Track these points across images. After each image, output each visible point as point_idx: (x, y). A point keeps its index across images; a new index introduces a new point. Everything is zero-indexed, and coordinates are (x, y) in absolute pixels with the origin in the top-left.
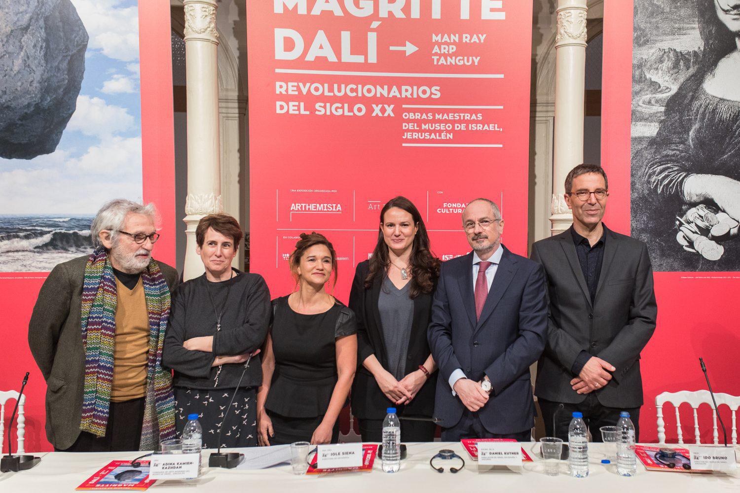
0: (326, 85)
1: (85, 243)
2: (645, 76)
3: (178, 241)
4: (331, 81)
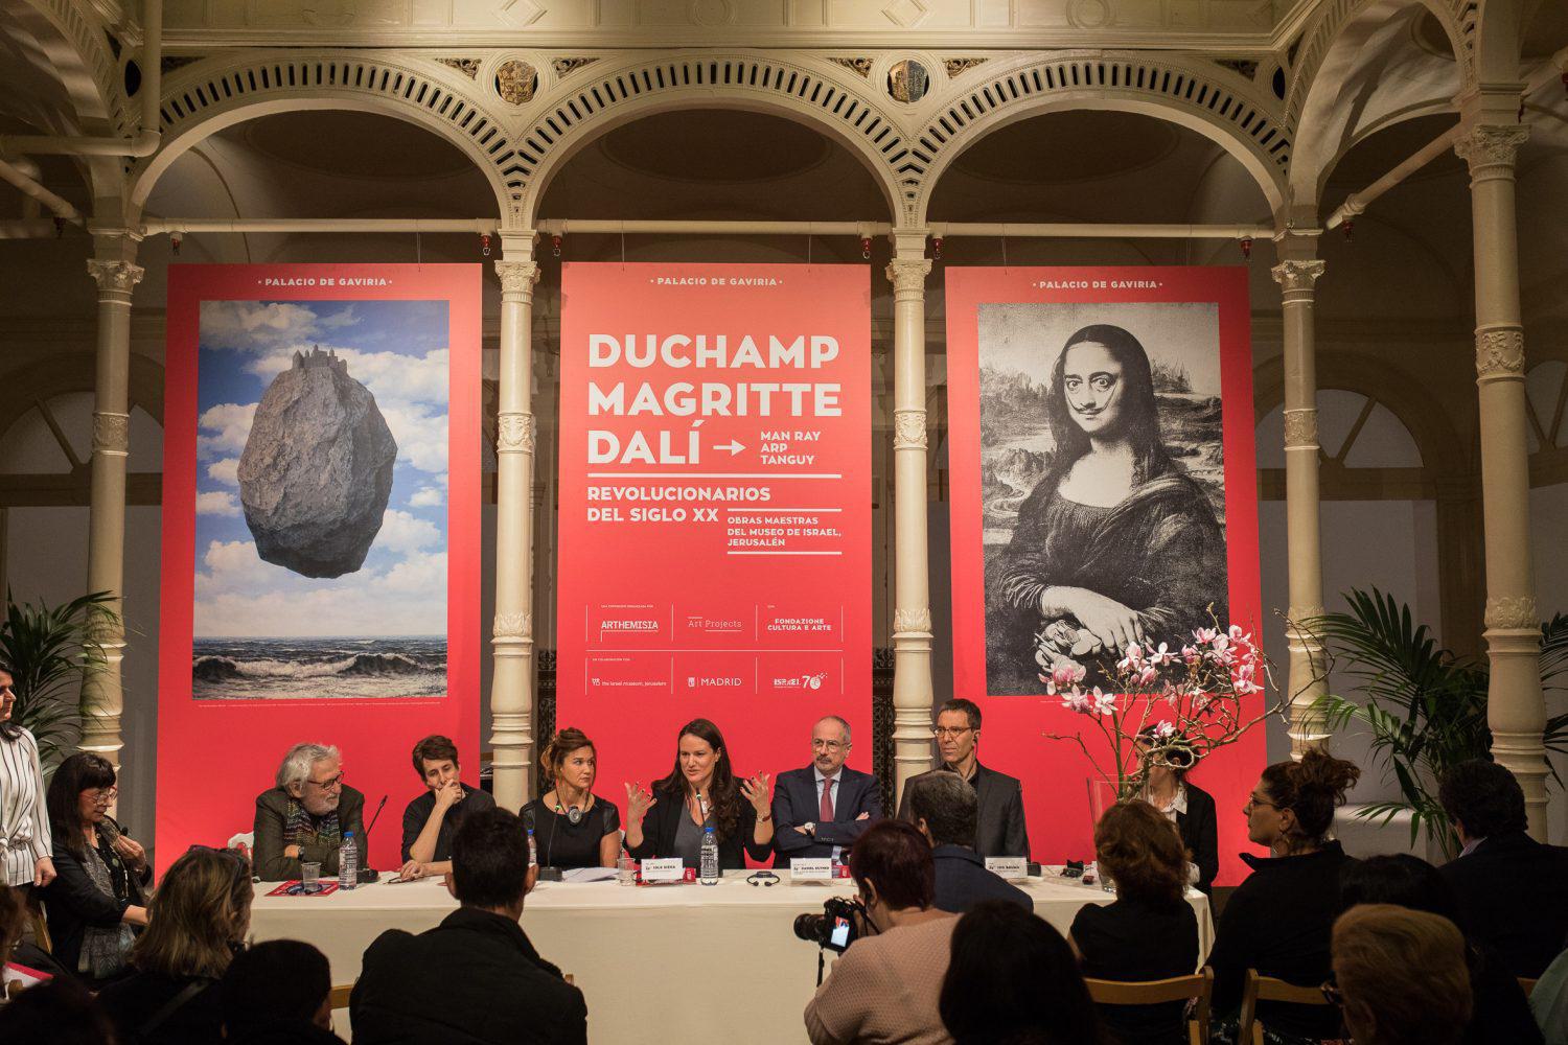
0: (643, 489)
1: (389, 667)
2: (996, 479)
3: (483, 667)
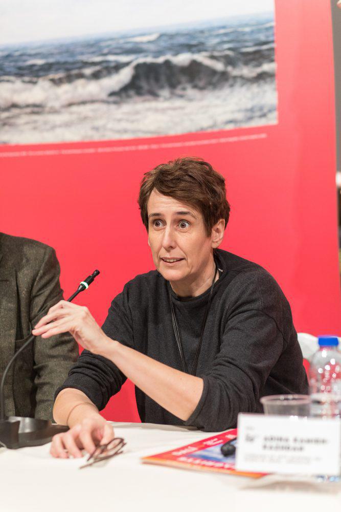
1: (183, 79)
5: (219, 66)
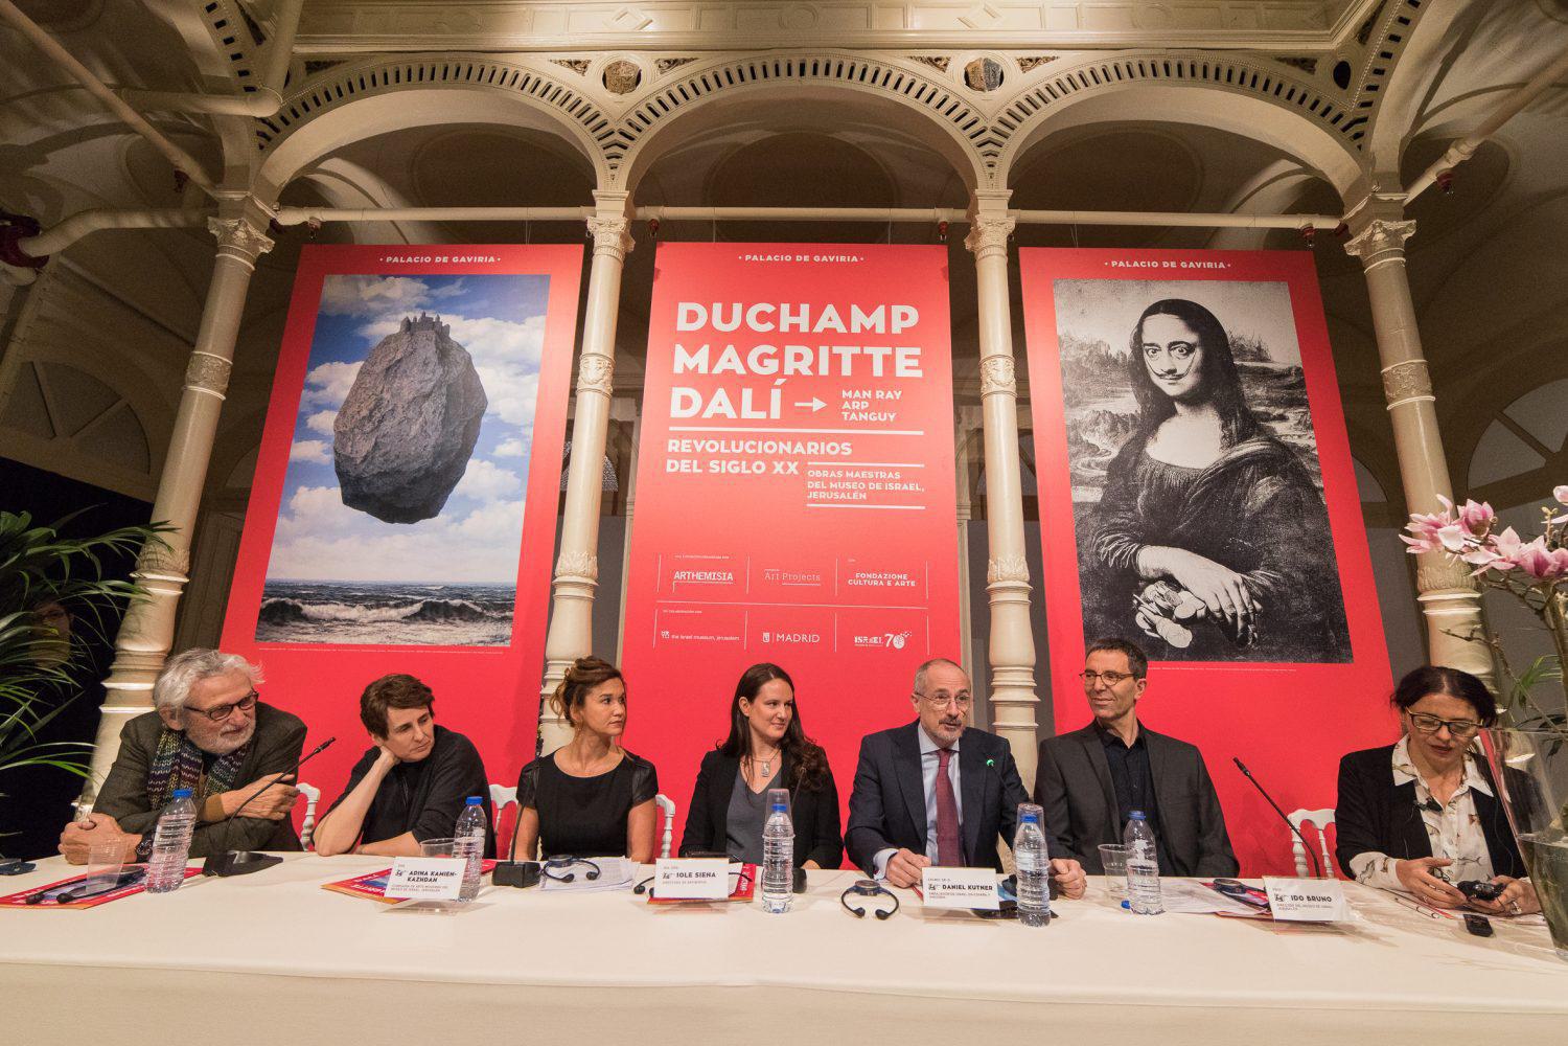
0: (723, 443)
1: (455, 614)
4: (727, 437)
5: (479, 609)
